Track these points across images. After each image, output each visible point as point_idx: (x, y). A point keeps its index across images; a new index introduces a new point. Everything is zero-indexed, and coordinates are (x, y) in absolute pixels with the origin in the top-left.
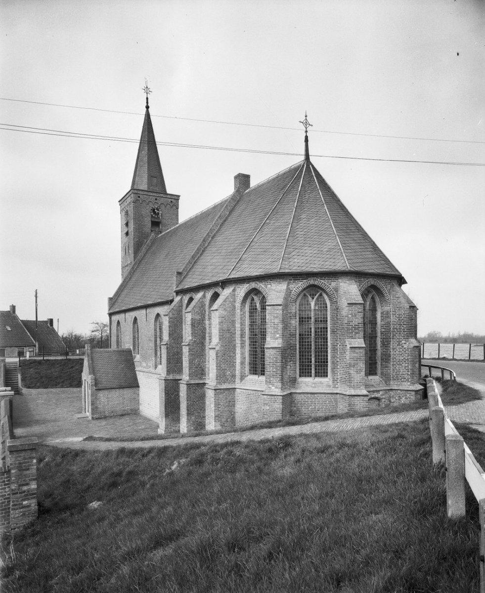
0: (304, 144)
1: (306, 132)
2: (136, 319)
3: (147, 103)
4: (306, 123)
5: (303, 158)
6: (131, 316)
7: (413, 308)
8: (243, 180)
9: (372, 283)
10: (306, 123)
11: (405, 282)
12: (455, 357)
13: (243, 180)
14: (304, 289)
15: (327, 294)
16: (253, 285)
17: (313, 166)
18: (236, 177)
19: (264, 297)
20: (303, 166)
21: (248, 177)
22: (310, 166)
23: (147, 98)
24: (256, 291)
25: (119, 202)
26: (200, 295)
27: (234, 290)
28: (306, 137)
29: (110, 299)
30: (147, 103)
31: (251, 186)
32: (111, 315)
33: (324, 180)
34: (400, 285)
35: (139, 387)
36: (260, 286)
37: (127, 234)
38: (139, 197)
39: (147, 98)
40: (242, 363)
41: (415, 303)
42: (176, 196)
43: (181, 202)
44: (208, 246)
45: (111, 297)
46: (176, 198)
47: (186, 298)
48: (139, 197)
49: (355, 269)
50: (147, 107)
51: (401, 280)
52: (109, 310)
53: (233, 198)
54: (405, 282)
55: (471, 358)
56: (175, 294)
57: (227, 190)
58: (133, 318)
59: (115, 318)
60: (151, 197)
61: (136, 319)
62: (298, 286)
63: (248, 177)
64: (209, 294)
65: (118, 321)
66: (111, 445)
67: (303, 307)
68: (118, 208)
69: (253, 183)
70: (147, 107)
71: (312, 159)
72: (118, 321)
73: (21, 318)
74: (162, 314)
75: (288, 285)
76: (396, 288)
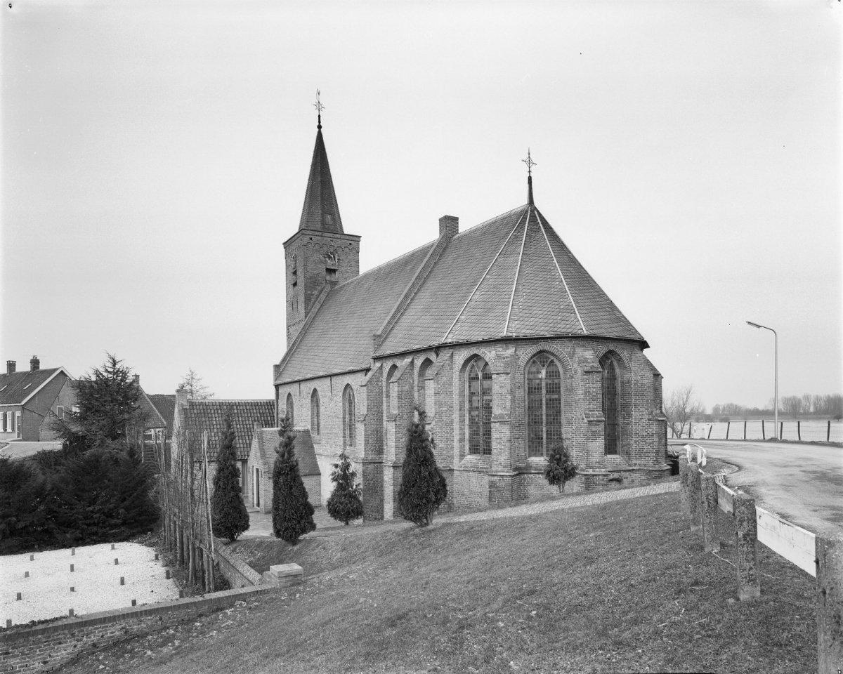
0: (527, 186)
1: (530, 171)
2: (315, 390)
3: (319, 122)
4: (529, 162)
5: (525, 201)
6: (307, 388)
7: (657, 376)
8: (449, 223)
9: (611, 348)
10: (529, 162)
11: (647, 346)
12: (802, 439)
13: (449, 223)
14: (534, 356)
15: (560, 360)
16: (474, 351)
17: (538, 211)
18: (441, 220)
19: (487, 364)
20: (527, 211)
21: (455, 220)
22: (536, 213)
23: (319, 116)
24: (475, 357)
25: (284, 244)
26: (408, 360)
27: (452, 356)
28: (530, 179)
29: (277, 367)
30: (319, 122)
31: (460, 231)
32: (277, 387)
33: (551, 228)
34: (642, 350)
35: (320, 474)
36: (480, 351)
37: (295, 284)
38: (311, 239)
39: (319, 116)
40: (462, 440)
41: (660, 370)
42: (356, 236)
43: (363, 245)
44: (410, 303)
45: (278, 364)
46: (357, 239)
47: (388, 365)
48: (311, 239)
49: (591, 331)
50: (320, 127)
51: (643, 345)
52: (276, 380)
53: (440, 243)
54: (647, 346)
55: (831, 440)
56: (372, 361)
57: (432, 234)
58: (312, 391)
59: (284, 391)
60: (325, 239)
61: (315, 390)
62: (526, 352)
63: (455, 220)
64: (419, 361)
65: (289, 394)
66: (525, 510)
67: (533, 374)
68: (282, 251)
69: (463, 228)
70: (320, 127)
71: (536, 204)
72: (289, 394)
73: (152, 393)
74: (352, 384)
75: (516, 350)
76: (639, 353)
